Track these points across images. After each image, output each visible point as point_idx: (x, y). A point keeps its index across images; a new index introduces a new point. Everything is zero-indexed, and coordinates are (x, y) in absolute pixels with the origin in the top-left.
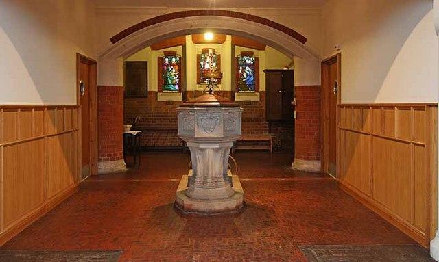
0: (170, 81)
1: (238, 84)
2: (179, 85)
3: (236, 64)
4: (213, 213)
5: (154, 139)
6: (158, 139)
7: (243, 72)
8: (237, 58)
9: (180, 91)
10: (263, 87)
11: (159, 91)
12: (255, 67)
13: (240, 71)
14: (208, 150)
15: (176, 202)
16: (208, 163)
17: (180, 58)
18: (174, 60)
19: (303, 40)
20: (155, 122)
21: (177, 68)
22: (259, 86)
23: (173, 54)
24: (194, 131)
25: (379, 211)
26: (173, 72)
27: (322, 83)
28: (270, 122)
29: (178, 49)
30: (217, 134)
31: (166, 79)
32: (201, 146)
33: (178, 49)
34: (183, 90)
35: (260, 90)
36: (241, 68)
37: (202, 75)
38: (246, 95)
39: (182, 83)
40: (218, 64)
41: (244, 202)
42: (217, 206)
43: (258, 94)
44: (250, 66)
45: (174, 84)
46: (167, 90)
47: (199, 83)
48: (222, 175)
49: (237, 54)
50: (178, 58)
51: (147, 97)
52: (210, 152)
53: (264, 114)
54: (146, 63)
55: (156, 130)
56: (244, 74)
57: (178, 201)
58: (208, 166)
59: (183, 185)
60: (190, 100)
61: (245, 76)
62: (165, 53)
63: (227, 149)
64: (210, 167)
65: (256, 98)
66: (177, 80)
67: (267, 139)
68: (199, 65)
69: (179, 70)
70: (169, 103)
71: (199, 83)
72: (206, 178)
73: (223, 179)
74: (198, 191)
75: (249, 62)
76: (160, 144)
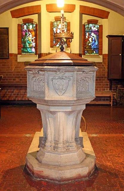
0: (27, 44)
1: (84, 48)
2: (36, 48)
3: (83, 30)
4: (63, 181)
5: (15, 94)
6: (17, 94)
7: (89, 38)
8: (84, 25)
9: (36, 54)
10: (105, 50)
11: (19, 54)
12: (99, 33)
13: (87, 37)
14: (59, 114)
15: (26, 165)
16: (59, 127)
17: (36, 25)
18: (31, 27)
20: (15, 80)
21: (33, 33)
22: (102, 49)
23: (30, 21)
24: (44, 93)
26: (30, 37)
28: (111, 81)
29: (35, 17)
31: (25, 43)
32: (52, 109)
33: (35, 17)
34: (38, 52)
35: (103, 53)
36: (87, 34)
37: (55, 39)
38: (91, 57)
39: (37, 47)
41: (95, 165)
42: (69, 174)
43: (101, 56)
44: (95, 32)
45: (31, 48)
46: (24, 52)
47: (52, 47)
48: (74, 140)
49: (84, 21)
50: (34, 25)
51: (8, 59)
53: (106, 74)
54: (7, 29)
55: (10, 87)
56: (90, 39)
57: (28, 164)
58: (59, 132)
59: (34, 147)
60: (42, 62)
61: (91, 41)
62: (24, 20)
63: (79, 111)
64: (61, 132)
65: (100, 59)
66: (34, 44)
67: (108, 95)
68: (52, 30)
69: (36, 35)
71: (52, 47)
72: (56, 142)
73: (74, 144)
74: (48, 156)
75: (94, 29)
76: (20, 99)
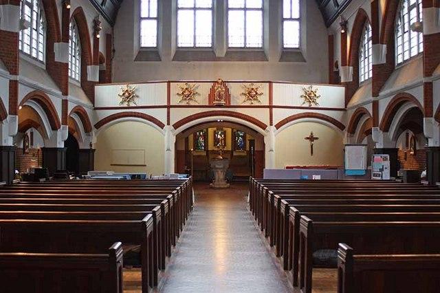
9: (205, 150)
19: (112, 165)
25: (318, 271)
26: (201, 140)
27: (157, 44)
30: (222, 166)
37: (216, 141)
40: (225, 136)
44: (241, 136)
52: (220, 172)
65: (244, 154)
70: (199, 156)
